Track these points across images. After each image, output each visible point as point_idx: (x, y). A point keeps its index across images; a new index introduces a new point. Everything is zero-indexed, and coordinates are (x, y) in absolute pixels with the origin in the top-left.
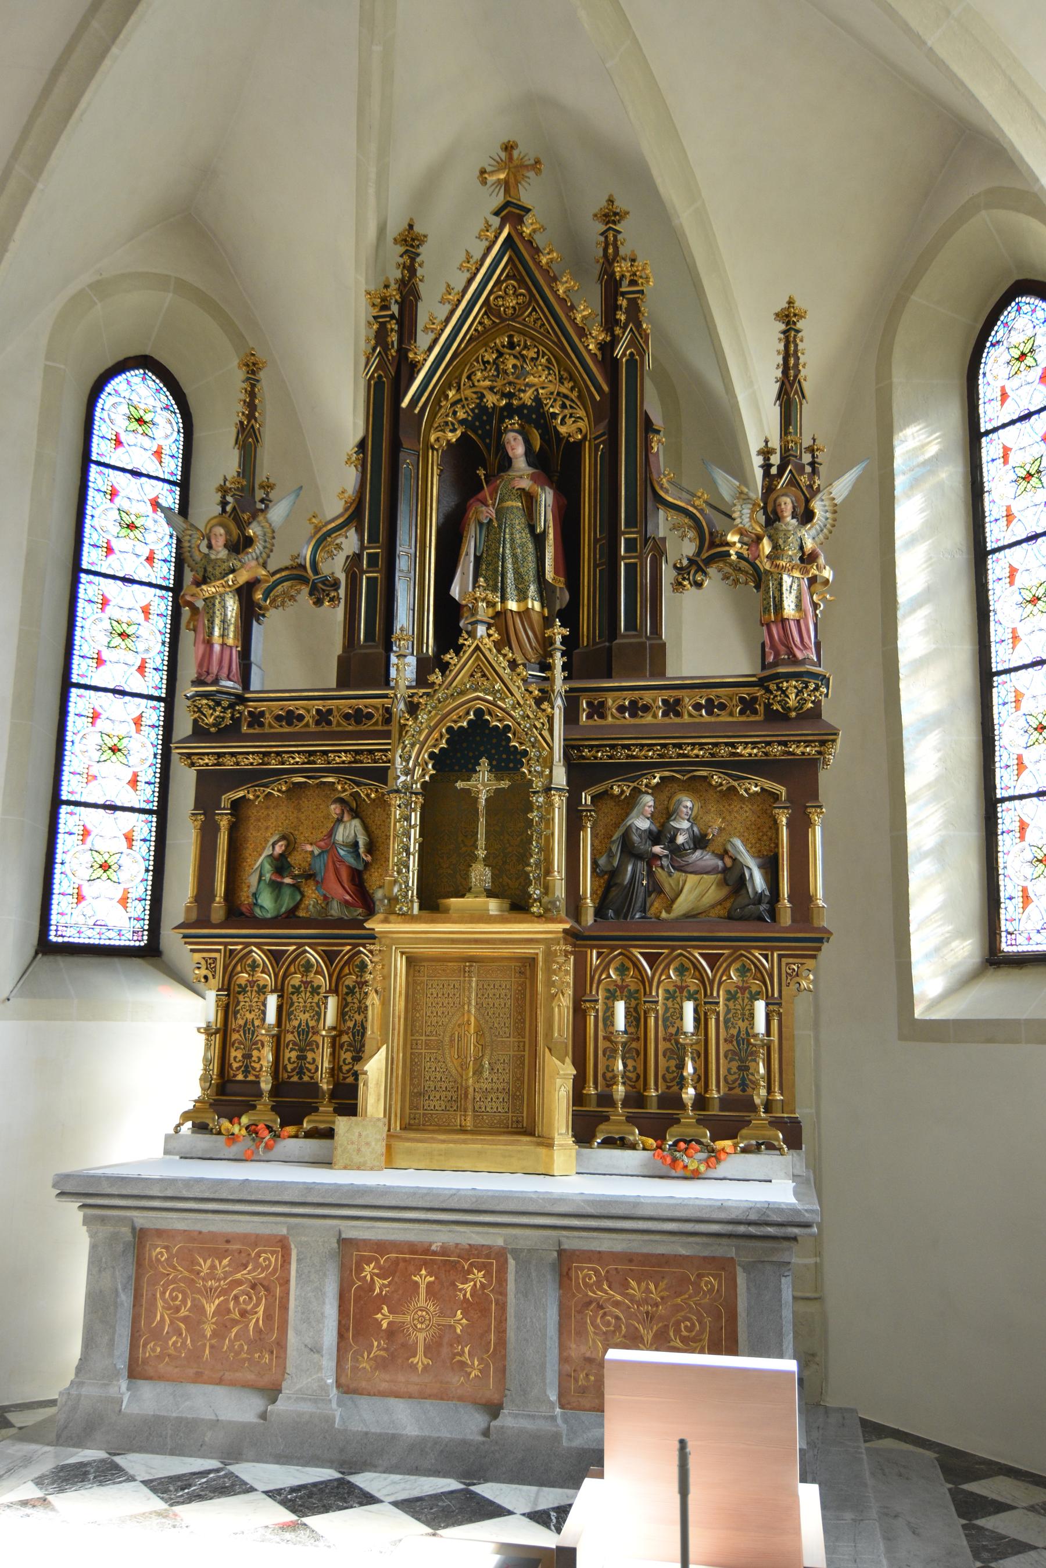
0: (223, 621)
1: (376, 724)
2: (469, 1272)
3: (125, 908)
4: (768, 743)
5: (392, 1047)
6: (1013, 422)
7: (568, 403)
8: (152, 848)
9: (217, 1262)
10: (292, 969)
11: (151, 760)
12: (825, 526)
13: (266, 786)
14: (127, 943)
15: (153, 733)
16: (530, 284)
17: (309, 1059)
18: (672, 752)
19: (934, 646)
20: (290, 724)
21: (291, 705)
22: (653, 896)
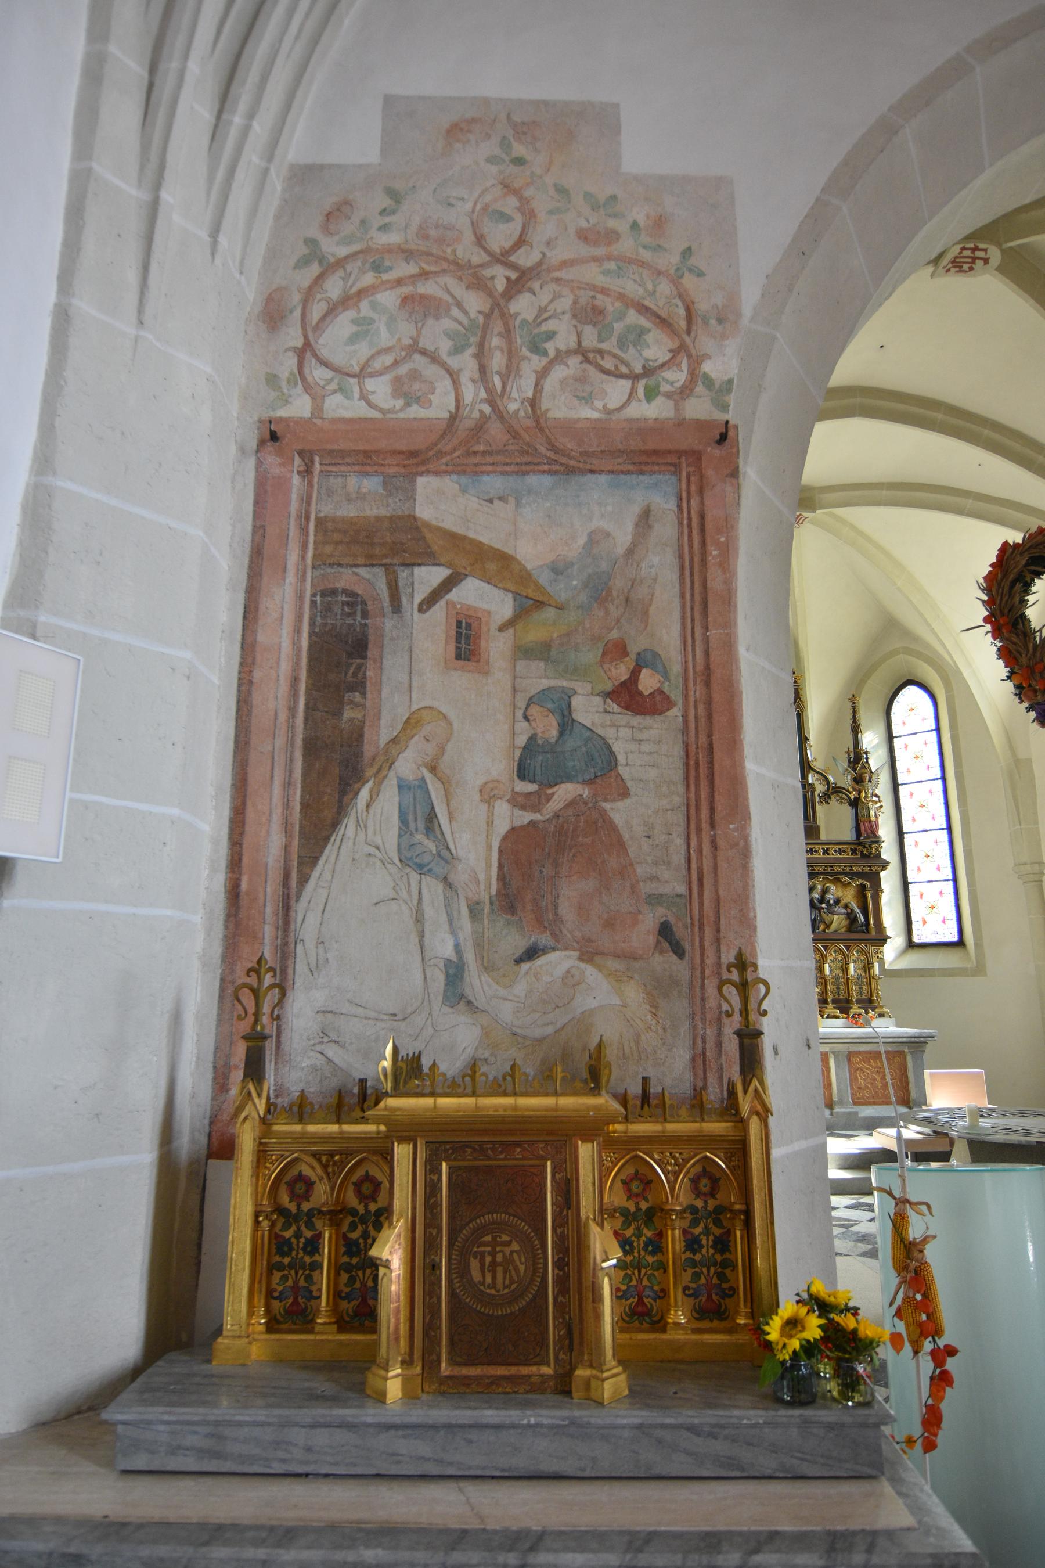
6: (146, 268)
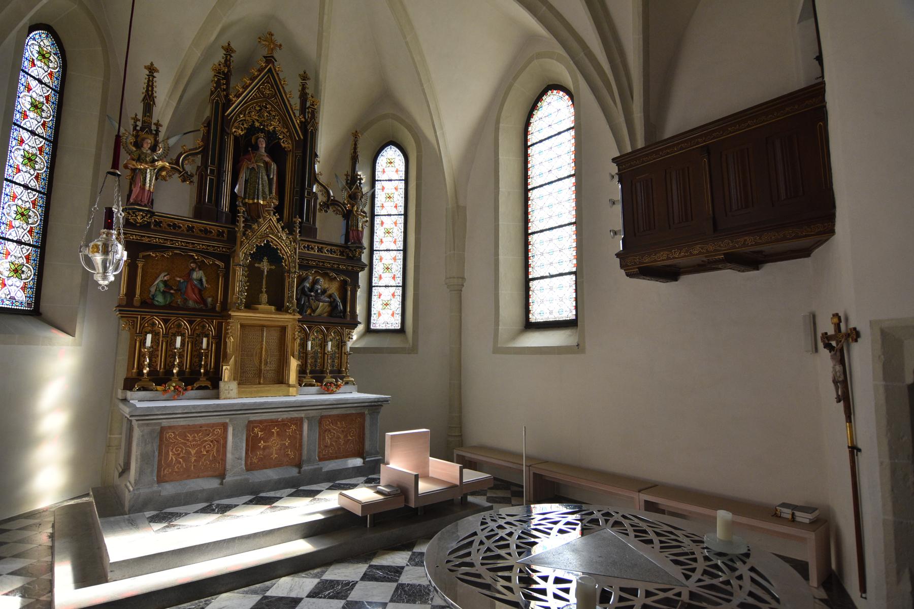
21: (176, 222)
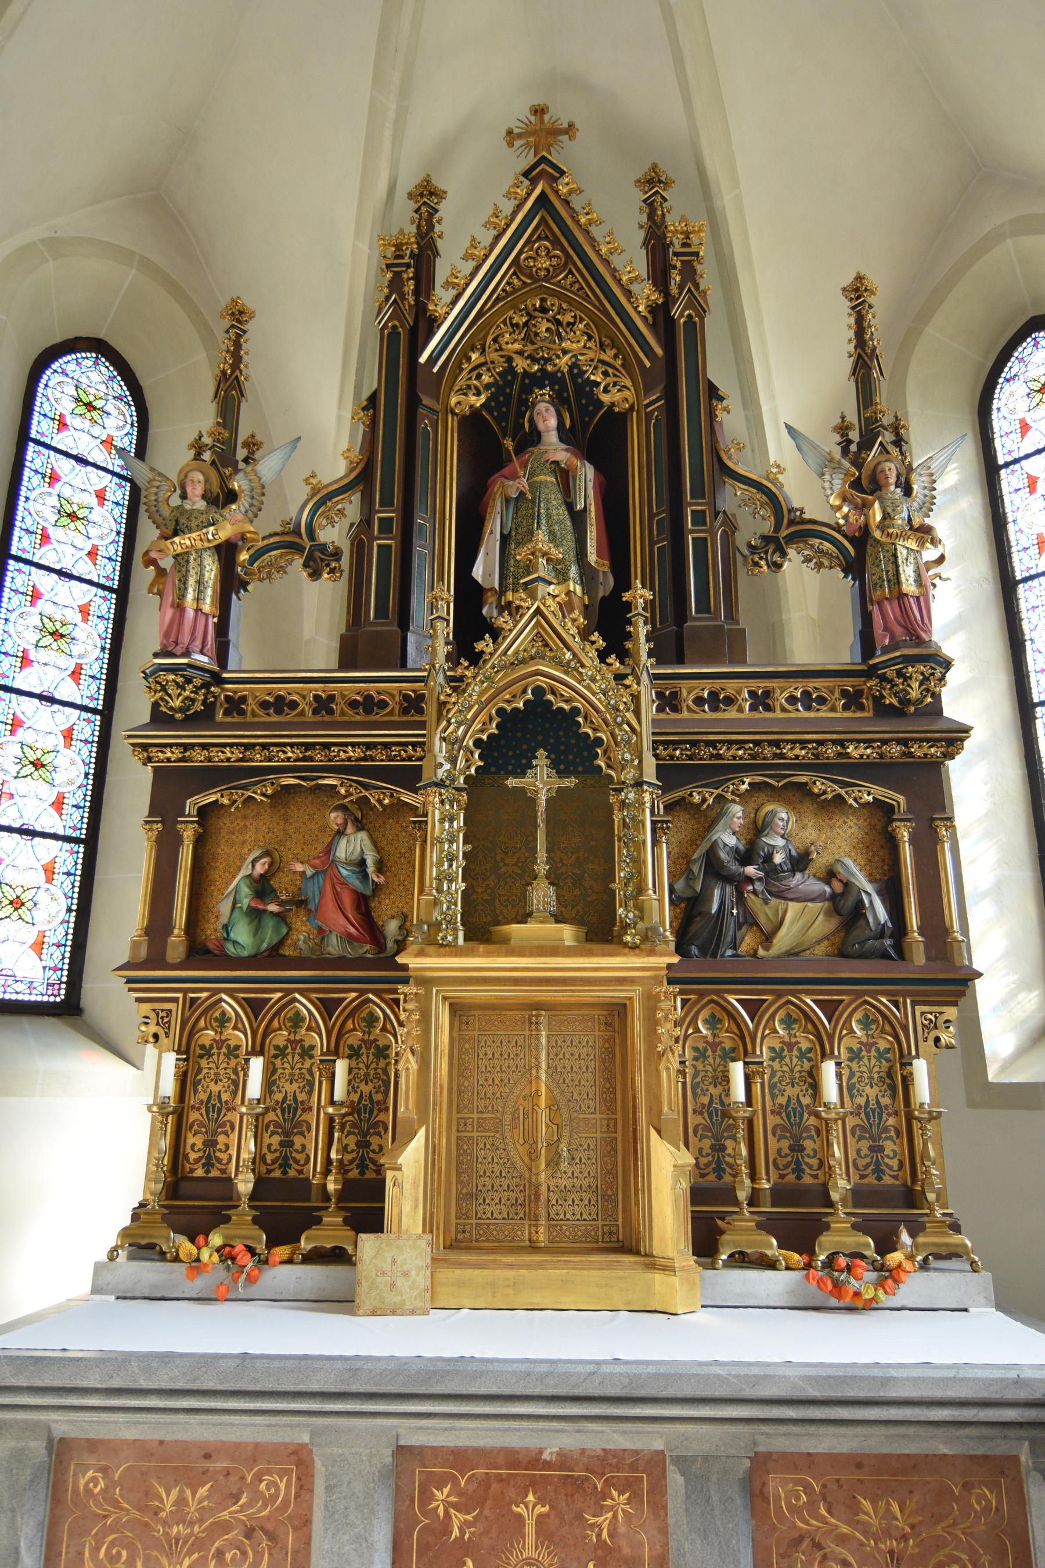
0: (199, 582)
1: (391, 713)
2: (605, 1495)
3: (39, 954)
4: (885, 742)
5: (434, 1129)
7: (610, 371)
8: (77, 884)
9: (188, 1492)
10: (276, 1024)
11: (81, 779)
12: (924, 503)
13: (244, 787)
14: (39, 998)
15: (85, 749)
16: (566, 244)
17: (297, 1146)
18: (768, 751)
19: (970, 675)
20: (279, 712)
22: (744, 929)
